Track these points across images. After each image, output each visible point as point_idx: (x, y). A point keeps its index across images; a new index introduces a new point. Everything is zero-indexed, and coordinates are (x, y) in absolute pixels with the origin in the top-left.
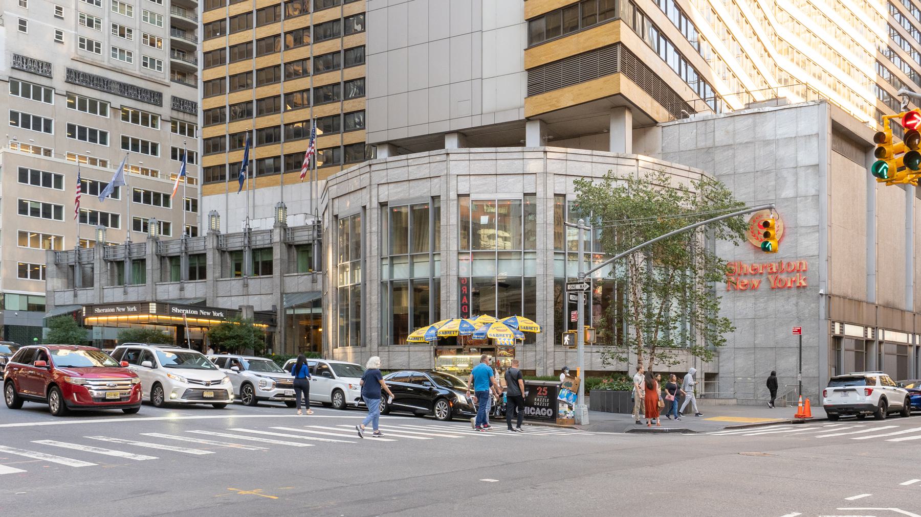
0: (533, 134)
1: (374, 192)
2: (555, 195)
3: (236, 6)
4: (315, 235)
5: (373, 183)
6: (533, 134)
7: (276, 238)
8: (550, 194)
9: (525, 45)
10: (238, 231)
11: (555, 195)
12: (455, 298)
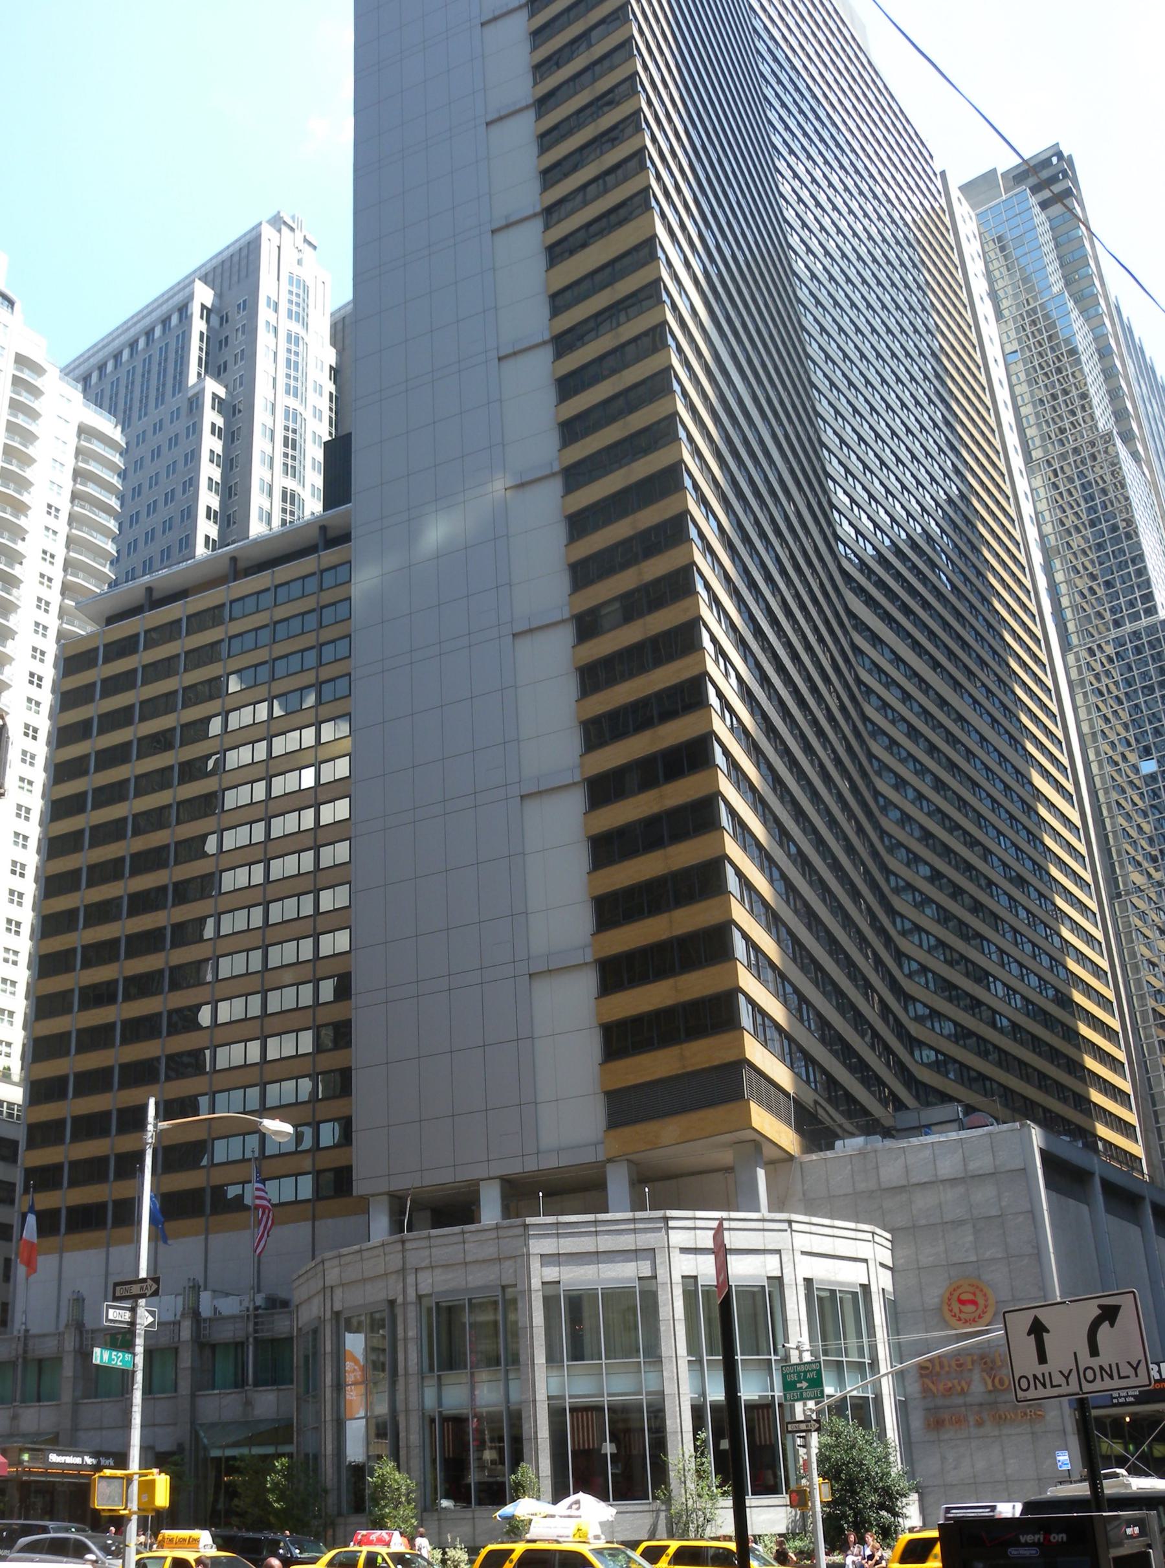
0: (618, 1183)
1: (411, 1279)
2: (683, 1277)
3: (135, 920)
4: (251, 1329)
5: (408, 1266)
6: (618, 1183)
7: (186, 1333)
8: (676, 1278)
9: (549, 317)
10: (86, 1315)
11: (683, 1277)
12: (549, 1473)
